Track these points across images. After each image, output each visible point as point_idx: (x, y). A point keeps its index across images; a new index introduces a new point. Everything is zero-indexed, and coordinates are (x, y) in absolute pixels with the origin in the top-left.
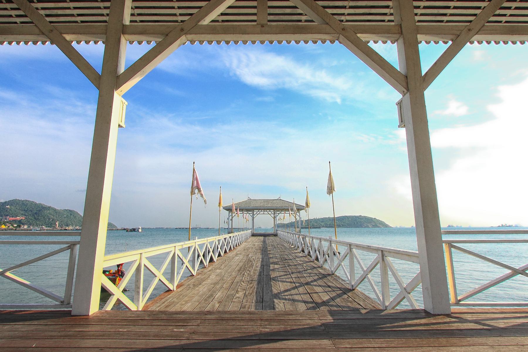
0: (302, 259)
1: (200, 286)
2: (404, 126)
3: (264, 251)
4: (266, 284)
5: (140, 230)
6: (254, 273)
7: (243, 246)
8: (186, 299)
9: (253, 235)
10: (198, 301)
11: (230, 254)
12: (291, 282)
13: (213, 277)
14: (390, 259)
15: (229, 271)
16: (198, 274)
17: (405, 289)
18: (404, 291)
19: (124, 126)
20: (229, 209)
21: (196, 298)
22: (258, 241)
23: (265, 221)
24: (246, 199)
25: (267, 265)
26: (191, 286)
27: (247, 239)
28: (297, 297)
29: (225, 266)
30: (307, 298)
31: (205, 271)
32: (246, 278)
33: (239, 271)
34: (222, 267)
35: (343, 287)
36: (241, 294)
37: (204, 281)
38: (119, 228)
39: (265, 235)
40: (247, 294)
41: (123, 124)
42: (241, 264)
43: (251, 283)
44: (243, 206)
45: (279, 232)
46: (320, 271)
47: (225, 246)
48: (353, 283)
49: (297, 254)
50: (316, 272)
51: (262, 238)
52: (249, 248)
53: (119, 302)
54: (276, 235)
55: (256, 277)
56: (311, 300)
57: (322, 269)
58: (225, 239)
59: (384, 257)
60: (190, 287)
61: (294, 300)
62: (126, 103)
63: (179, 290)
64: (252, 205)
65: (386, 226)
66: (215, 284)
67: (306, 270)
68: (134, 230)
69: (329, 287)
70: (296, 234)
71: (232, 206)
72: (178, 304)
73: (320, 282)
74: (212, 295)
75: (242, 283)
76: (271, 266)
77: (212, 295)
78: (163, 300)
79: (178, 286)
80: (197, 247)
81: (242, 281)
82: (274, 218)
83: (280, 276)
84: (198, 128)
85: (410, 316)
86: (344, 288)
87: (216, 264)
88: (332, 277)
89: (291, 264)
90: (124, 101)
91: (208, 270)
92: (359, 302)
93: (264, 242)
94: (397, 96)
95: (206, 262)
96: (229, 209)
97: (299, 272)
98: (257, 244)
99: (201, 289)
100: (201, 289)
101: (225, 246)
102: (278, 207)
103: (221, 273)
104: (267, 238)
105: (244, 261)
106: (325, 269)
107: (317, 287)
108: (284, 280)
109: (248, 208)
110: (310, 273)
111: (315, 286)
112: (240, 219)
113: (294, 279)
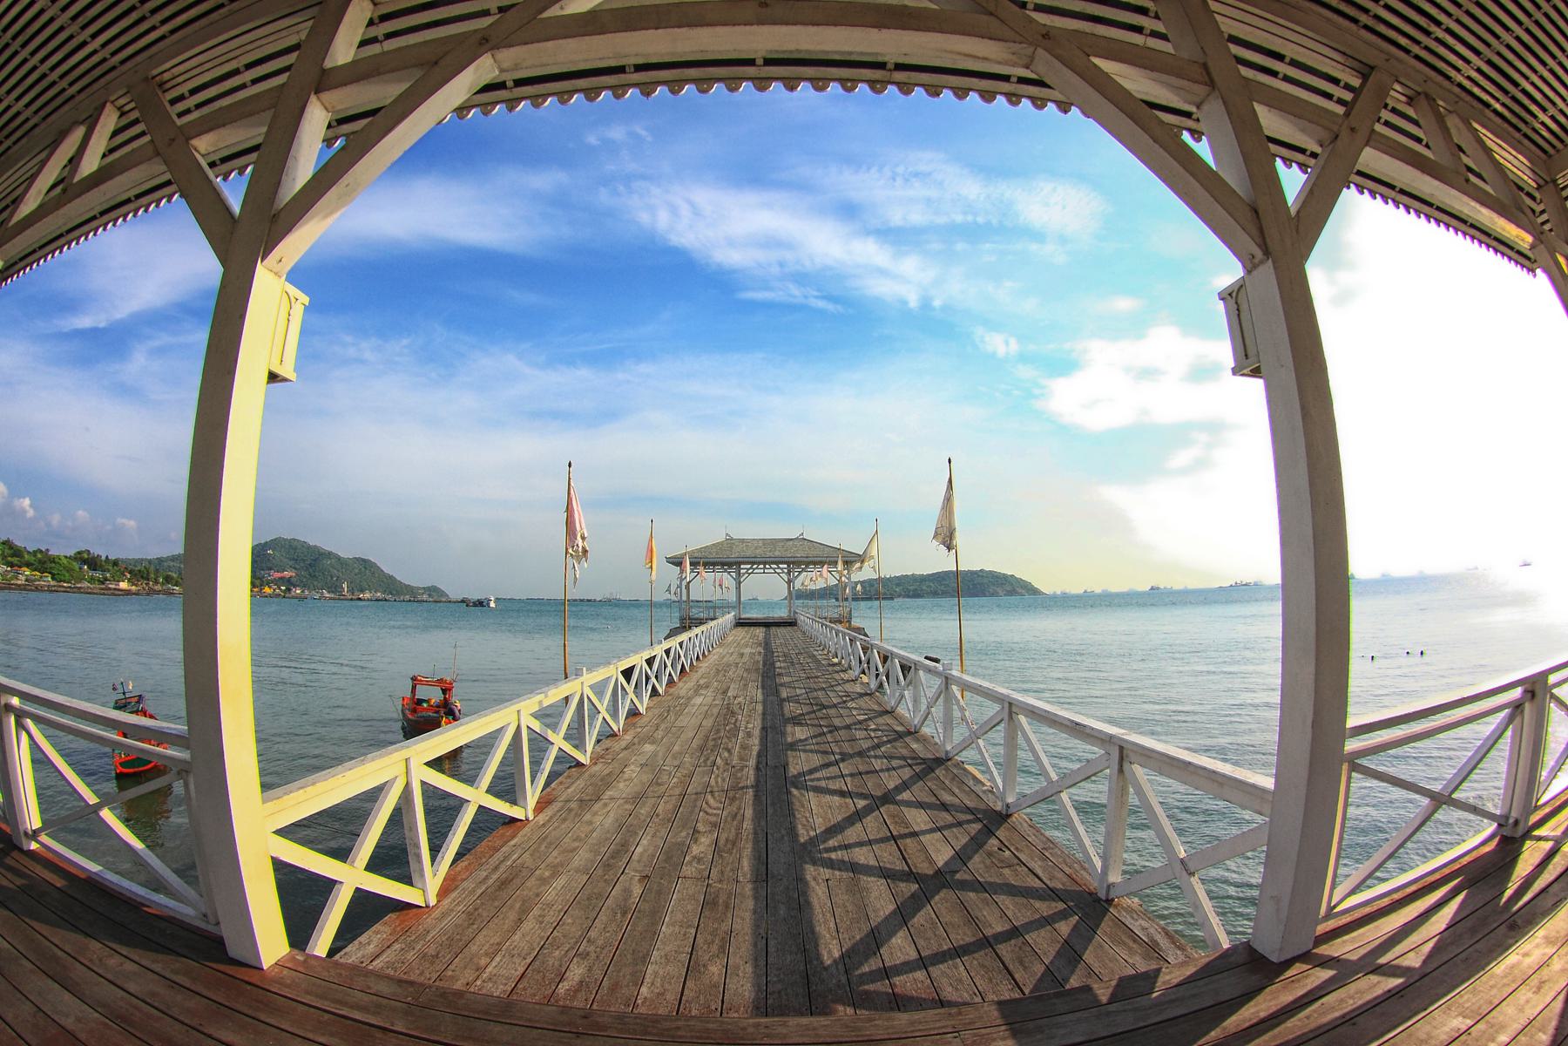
0: (862, 702)
1: (597, 806)
2: (1256, 373)
3: (768, 674)
4: (773, 804)
5: (492, 605)
6: (741, 759)
7: (713, 658)
8: (555, 857)
9: (741, 623)
10: (585, 871)
11: (684, 688)
12: (842, 794)
13: (632, 771)
14: (1139, 771)
15: (676, 748)
16: (595, 759)
17: (1182, 861)
18: (1178, 866)
19: (292, 376)
20: (677, 562)
21: (582, 857)
22: (748, 643)
23: (766, 589)
24: (721, 538)
25: (773, 728)
26: (573, 805)
27: (723, 637)
28: (862, 856)
29: (668, 731)
30: (888, 856)
31: (617, 745)
32: (720, 780)
33: (702, 749)
34: (659, 734)
35: (982, 807)
36: (702, 847)
37: (608, 786)
38: (455, 594)
39: (767, 624)
40: (722, 842)
41: (287, 370)
42: (708, 723)
43: (733, 799)
44: (713, 557)
45: (801, 618)
46: (914, 746)
47: (669, 668)
48: (1010, 800)
49: (848, 687)
50: (904, 752)
51: (760, 632)
52: (729, 665)
53: (373, 866)
54: (791, 623)
55: (749, 776)
56: (900, 866)
57: (917, 740)
58: (667, 652)
59: (1126, 766)
60: (570, 810)
61: (854, 868)
62: (306, 299)
63: (542, 818)
64: (734, 556)
65: (1034, 591)
66: (638, 798)
67: (878, 746)
68: (480, 603)
69: (944, 807)
70: (844, 634)
71: (682, 556)
72: (533, 879)
73: (918, 792)
74: (624, 846)
75: (709, 797)
76: (789, 729)
77: (624, 846)
78: (499, 855)
79: (539, 808)
80: (588, 692)
81: (707, 789)
82: (789, 582)
83: (811, 772)
84: (584, 372)
85: (1228, 986)
86: (985, 812)
87: (645, 720)
88: (947, 769)
89: (837, 722)
90: (294, 291)
91: (623, 744)
92: (1031, 865)
93: (767, 644)
94: (1230, 271)
95: (617, 722)
96: (677, 562)
97: (861, 754)
98: (747, 651)
99: (598, 820)
100: (598, 820)
101: (669, 668)
102: (795, 557)
103: (655, 754)
104: (773, 629)
105: (715, 711)
106: (924, 740)
107: (914, 811)
108: (823, 784)
109: (725, 559)
110: (890, 758)
111: (908, 804)
112: (706, 585)
113: (848, 779)
